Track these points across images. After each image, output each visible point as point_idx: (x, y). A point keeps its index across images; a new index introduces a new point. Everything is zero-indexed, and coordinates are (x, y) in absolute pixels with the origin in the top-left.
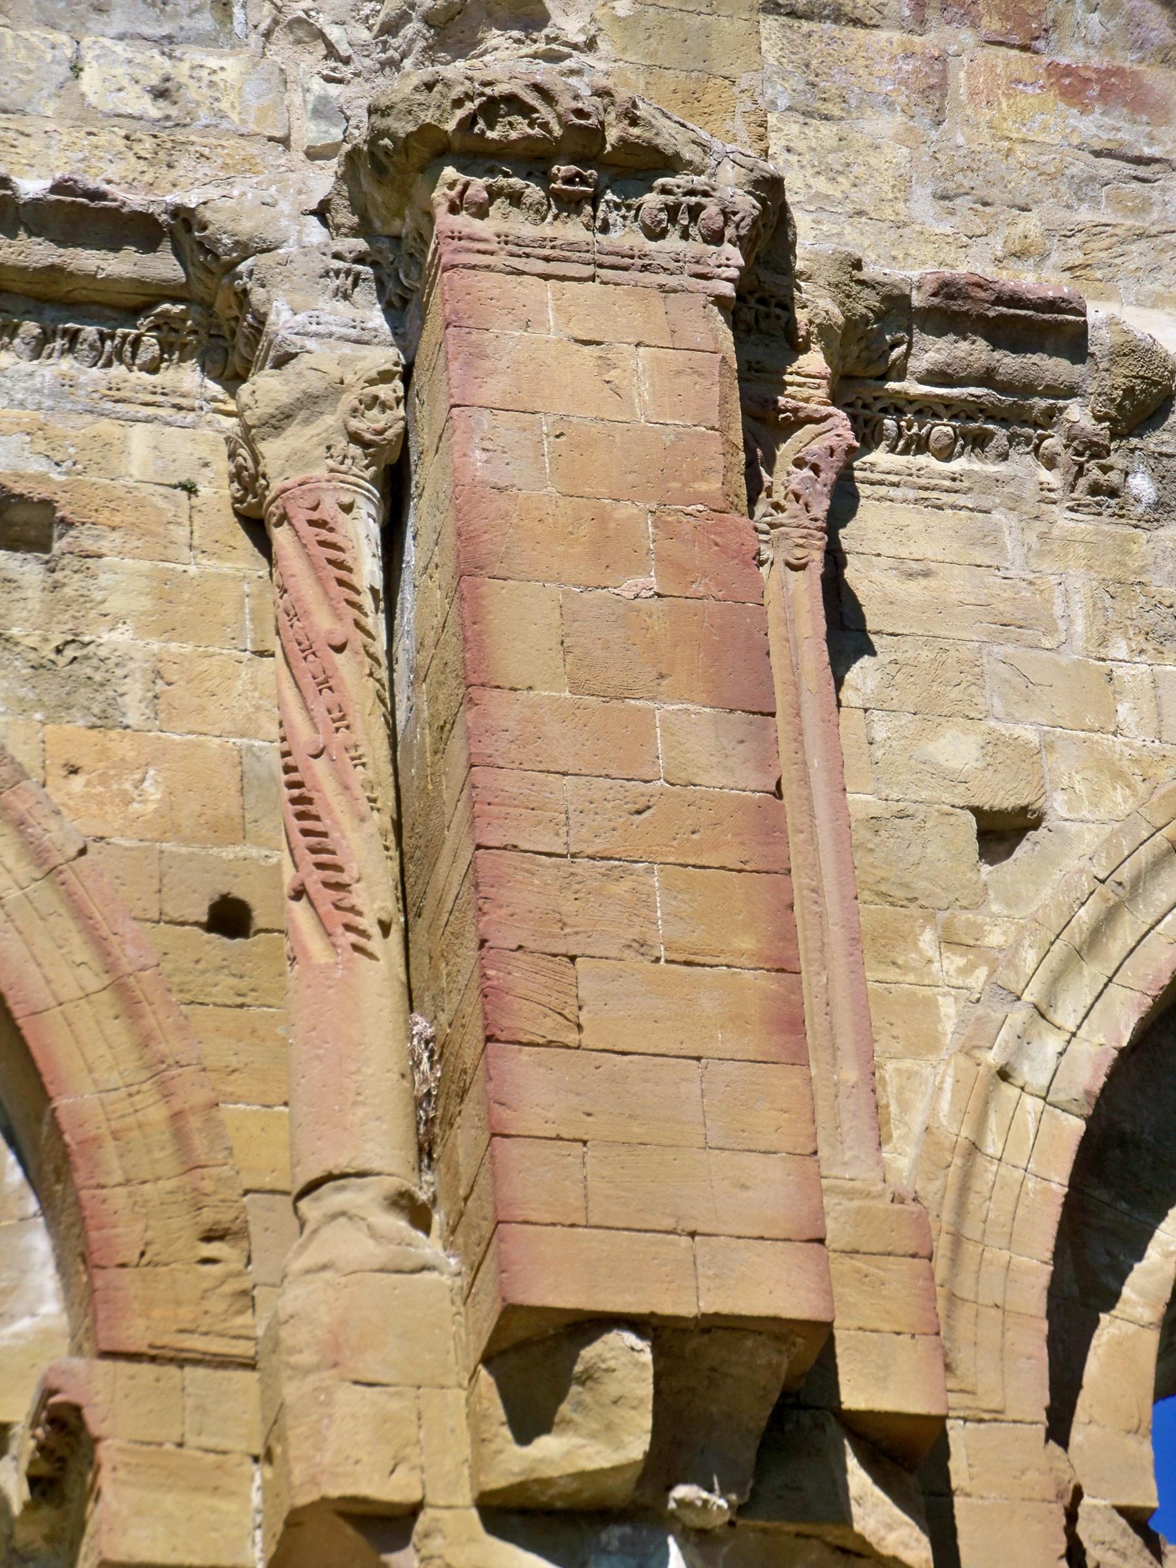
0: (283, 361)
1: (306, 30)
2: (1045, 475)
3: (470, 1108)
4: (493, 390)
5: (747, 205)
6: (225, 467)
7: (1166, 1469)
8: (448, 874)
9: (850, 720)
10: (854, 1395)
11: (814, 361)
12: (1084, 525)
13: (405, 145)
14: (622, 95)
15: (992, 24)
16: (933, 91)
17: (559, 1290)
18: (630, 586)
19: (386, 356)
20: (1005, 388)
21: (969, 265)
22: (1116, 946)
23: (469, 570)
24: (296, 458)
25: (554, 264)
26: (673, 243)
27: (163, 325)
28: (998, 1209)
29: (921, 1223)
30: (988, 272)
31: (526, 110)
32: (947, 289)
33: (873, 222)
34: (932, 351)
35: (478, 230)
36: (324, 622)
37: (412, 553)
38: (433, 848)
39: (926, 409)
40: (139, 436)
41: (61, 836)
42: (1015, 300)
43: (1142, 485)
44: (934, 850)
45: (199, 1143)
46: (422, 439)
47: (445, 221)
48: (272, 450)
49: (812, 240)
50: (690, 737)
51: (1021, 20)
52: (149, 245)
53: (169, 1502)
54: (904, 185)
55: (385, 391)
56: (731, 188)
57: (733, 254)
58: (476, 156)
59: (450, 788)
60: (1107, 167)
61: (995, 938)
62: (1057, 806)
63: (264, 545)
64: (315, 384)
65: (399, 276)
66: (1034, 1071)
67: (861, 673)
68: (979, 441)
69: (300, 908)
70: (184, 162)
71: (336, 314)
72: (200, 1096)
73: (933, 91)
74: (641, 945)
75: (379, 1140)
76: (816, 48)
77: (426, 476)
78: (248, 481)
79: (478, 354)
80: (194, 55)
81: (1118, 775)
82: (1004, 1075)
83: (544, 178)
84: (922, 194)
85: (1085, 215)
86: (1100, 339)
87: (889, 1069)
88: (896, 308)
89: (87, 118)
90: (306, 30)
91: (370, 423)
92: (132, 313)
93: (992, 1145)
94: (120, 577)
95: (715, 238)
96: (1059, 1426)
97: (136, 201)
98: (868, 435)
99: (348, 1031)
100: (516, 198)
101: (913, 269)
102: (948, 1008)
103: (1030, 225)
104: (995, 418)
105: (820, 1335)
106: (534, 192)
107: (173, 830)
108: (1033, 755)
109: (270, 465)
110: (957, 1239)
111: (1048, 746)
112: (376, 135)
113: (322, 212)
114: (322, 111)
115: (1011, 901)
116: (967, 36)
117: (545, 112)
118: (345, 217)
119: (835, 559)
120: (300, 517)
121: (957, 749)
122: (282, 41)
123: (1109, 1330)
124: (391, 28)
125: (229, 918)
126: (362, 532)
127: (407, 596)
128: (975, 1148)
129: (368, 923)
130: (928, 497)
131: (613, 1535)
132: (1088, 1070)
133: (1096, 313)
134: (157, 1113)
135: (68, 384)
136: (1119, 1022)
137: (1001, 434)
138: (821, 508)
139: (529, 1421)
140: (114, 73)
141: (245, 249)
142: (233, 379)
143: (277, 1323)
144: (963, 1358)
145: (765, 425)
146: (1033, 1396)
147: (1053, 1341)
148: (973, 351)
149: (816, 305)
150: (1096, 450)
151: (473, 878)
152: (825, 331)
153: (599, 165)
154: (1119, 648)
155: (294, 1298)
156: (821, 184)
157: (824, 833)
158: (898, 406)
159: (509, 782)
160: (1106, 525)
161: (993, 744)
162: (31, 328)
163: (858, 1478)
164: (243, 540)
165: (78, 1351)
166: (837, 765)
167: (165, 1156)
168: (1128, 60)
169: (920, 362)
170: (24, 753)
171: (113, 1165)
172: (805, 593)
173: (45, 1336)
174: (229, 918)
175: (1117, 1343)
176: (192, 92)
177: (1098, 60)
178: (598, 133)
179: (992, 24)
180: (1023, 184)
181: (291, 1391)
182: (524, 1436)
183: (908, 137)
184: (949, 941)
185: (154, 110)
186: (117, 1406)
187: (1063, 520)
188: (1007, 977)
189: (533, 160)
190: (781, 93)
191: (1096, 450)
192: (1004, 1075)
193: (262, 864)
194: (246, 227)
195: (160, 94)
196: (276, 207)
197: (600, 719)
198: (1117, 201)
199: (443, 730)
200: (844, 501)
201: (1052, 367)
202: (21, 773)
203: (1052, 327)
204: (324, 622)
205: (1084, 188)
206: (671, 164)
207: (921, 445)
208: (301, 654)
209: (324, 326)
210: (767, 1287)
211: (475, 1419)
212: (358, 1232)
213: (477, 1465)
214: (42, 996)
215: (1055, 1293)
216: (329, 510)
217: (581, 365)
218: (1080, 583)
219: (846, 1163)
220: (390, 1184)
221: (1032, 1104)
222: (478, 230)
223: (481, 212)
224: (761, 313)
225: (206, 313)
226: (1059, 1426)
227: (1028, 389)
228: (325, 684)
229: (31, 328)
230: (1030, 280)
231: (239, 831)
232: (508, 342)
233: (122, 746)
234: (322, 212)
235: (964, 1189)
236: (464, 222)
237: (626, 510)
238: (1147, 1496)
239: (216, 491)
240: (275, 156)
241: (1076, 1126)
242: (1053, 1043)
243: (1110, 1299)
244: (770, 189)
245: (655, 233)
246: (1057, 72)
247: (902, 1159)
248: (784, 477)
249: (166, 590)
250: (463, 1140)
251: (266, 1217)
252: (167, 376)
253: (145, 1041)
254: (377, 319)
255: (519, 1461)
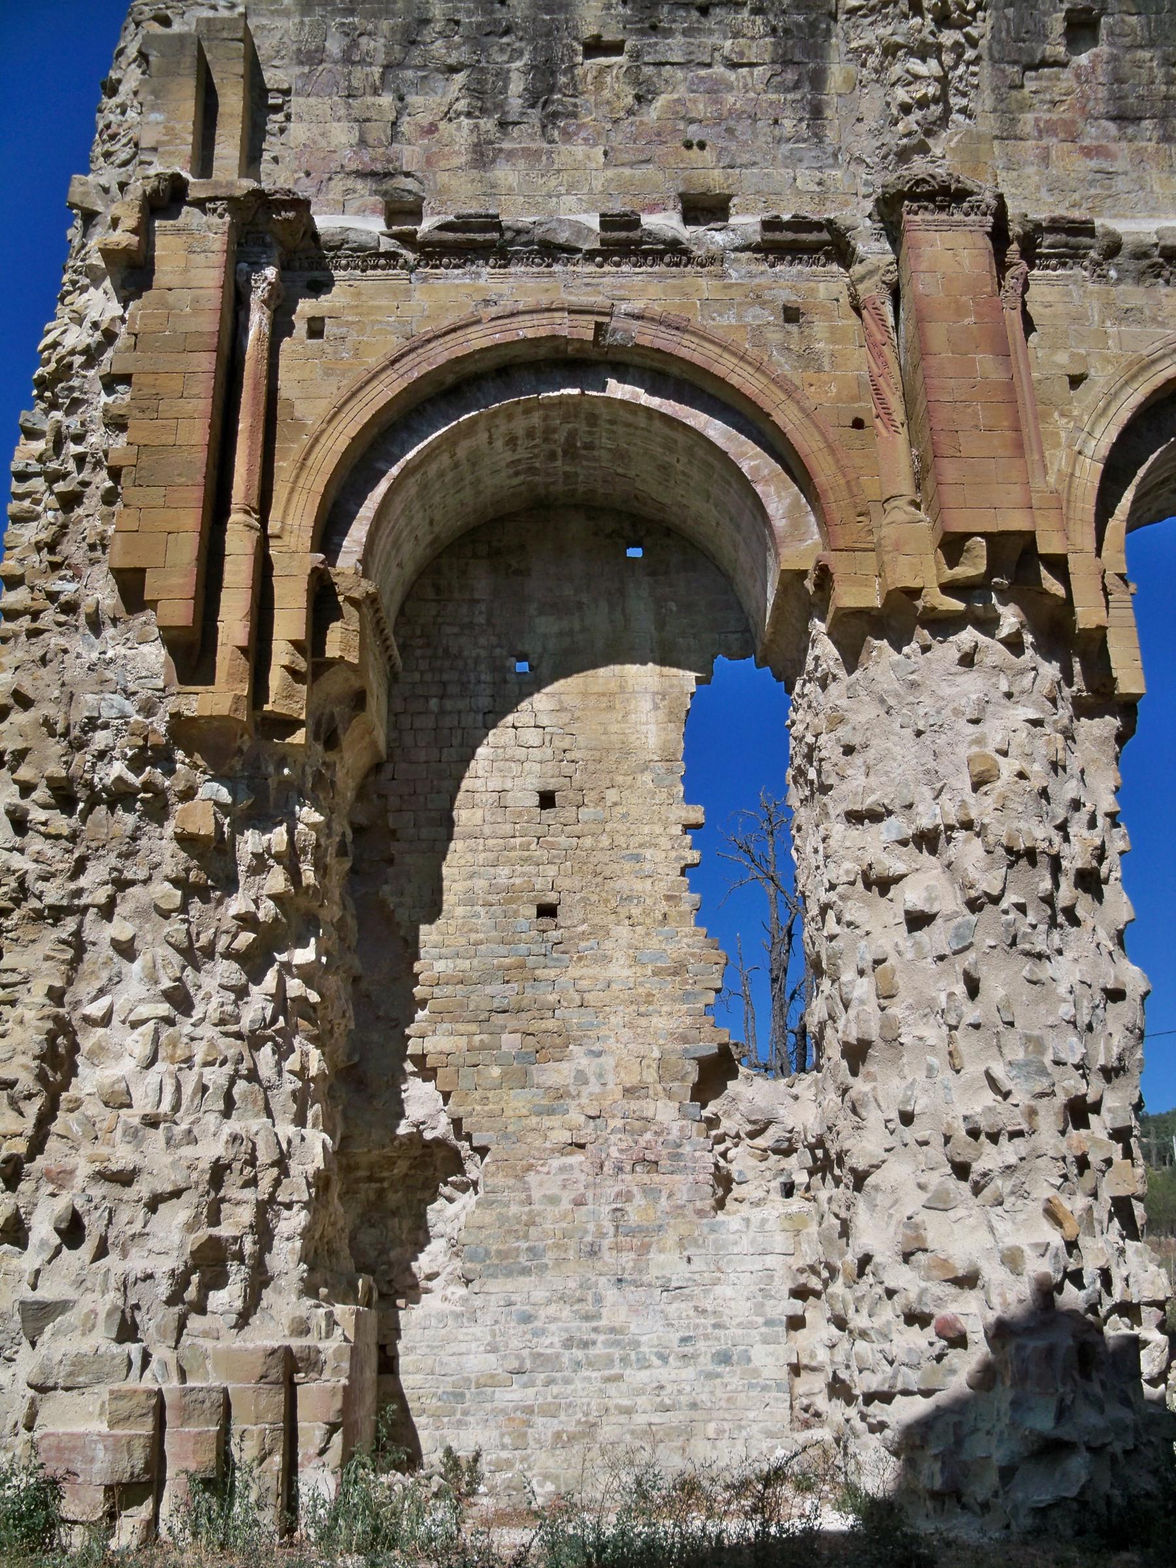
0: (861, 262)
1: (860, 160)
2: (1085, 273)
3: (930, 475)
4: (924, 266)
5: (994, 203)
6: (846, 293)
7: (1129, 562)
8: (920, 408)
9: (1031, 352)
10: (1042, 550)
11: (1015, 247)
12: (1096, 287)
13: (893, 196)
14: (955, 174)
15: (1062, 135)
16: (1045, 158)
17: (959, 525)
18: (966, 321)
19: (891, 257)
20: (1071, 248)
21: (1060, 212)
22: (1111, 412)
23: (920, 320)
24: (867, 290)
25: (938, 227)
26: (972, 217)
27: (826, 253)
28: (1079, 492)
29: (1059, 500)
30: (1065, 213)
31: (928, 182)
32: (1053, 220)
33: (1030, 204)
34: (1049, 239)
35: (917, 220)
36: (879, 337)
37: (902, 315)
38: (915, 400)
39: (1048, 256)
40: (822, 286)
41: (807, 404)
42: (1073, 222)
43: (1113, 273)
44: (1057, 388)
45: (855, 490)
46: (904, 281)
47: (906, 217)
48: (860, 287)
49: (1012, 211)
50: (986, 364)
51: (1071, 134)
52: (820, 230)
53: (854, 590)
54: (1038, 188)
55: (891, 268)
56: (989, 199)
57: (990, 219)
58: (913, 196)
59: (918, 385)
60: (1099, 176)
61: (1076, 413)
62: (1092, 372)
63: (860, 315)
64: (871, 267)
65: (893, 231)
66: (1089, 452)
67: (1033, 337)
68: (1064, 265)
69: (878, 421)
70: (828, 203)
71: (875, 246)
72: (854, 476)
73: (1045, 158)
74: (976, 427)
75: (905, 486)
76: (1010, 148)
77: (905, 292)
78: (854, 297)
79: (919, 256)
80: (828, 171)
81: (1109, 362)
82: (1080, 453)
83: (934, 202)
84: (1044, 190)
85: (1093, 191)
86: (1099, 231)
87: (1047, 453)
88: (1038, 227)
89: (799, 193)
90: (860, 160)
91: (888, 277)
92: (816, 251)
93: (1077, 474)
94: (820, 327)
95: (985, 214)
96: (1098, 552)
97: (815, 218)
98: (1032, 266)
99: (895, 453)
100: (926, 208)
101: (1042, 215)
102: (1063, 434)
103: (1076, 196)
104: (1070, 256)
105: (1032, 534)
106: (931, 206)
107: (840, 400)
108: (1083, 358)
109: (860, 292)
110: (1069, 501)
111: (1088, 355)
112: (884, 193)
113: (870, 216)
114: (867, 183)
115: (1080, 402)
116: (1055, 140)
117: (933, 182)
118: (877, 218)
119: (1024, 304)
120: (870, 307)
121: (1062, 358)
122: (853, 163)
123: (1111, 522)
124: (885, 157)
125: (858, 424)
126: (888, 309)
127: (902, 326)
128: (1072, 474)
129: (898, 424)
130: (1050, 282)
131: (978, 592)
132: (1104, 451)
133: (1098, 222)
134: (842, 482)
135: (800, 273)
136: (1112, 435)
137: (1071, 262)
138: (1020, 290)
139: (952, 562)
140: (806, 179)
141: (848, 229)
142: (847, 267)
143: (880, 539)
144: (1071, 535)
145: (1002, 267)
146: (1091, 545)
147: (1097, 528)
148: (1062, 238)
149: (1015, 229)
150: (1099, 264)
151: (928, 411)
152: (1018, 238)
153: (947, 196)
154: (1108, 324)
155: (885, 531)
156: (1013, 190)
157: (1026, 388)
158: (1040, 256)
159: (936, 382)
160: (1103, 287)
161: (1073, 355)
162: (789, 258)
163: (1044, 572)
164: (854, 314)
165: (825, 549)
166: (1028, 367)
167: (845, 493)
168: (1104, 142)
169: (1045, 243)
170: (797, 382)
171: (831, 497)
172: (1016, 315)
173: (815, 544)
174: (858, 424)
175: (1114, 527)
176: (828, 183)
177: (1095, 143)
178: (949, 187)
179: (1062, 135)
180: (1074, 184)
181: (886, 558)
182: (951, 568)
183: (1039, 173)
184: (1062, 415)
185: (818, 189)
186: (838, 565)
187: (1090, 286)
188: (1079, 424)
189: (930, 196)
190: (1000, 163)
191: (1099, 264)
192: (1080, 453)
193: (866, 407)
194: (848, 223)
195: (819, 184)
196: (857, 216)
197: (963, 373)
198: (1102, 186)
199: (915, 367)
200: (1026, 286)
201: (1086, 240)
202: (797, 388)
203: (1084, 229)
204: (879, 337)
205: (1092, 183)
206: (971, 193)
207: (1047, 267)
208: (874, 347)
209: (872, 249)
210: (1017, 522)
211: (937, 563)
212: (901, 512)
213: (938, 576)
214: (808, 451)
215: (1097, 515)
216: (878, 304)
217: (949, 251)
218: (1096, 305)
219: (1037, 483)
220: (909, 498)
221: (1088, 461)
222: (917, 220)
223: (916, 213)
224: (999, 235)
225: (836, 247)
226: (1098, 552)
227: (1078, 248)
228: (881, 355)
229: (789, 258)
230: (1077, 214)
231: (858, 398)
232: (926, 251)
233: (824, 377)
234: (870, 216)
235: (1070, 486)
236: (911, 217)
237: (964, 298)
238: (1124, 570)
239: (845, 300)
240: (855, 199)
241: (1101, 466)
242: (1094, 443)
243: (1111, 514)
244: (1000, 198)
245: (967, 215)
246: (1082, 148)
247: (1052, 479)
248: (1009, 282)
249: (833, 330)
250: (929, 484)
251: (875, 509)
252: (828, 268)
253: (837, 461)
254: (888, 247)
255: (949, 574)
